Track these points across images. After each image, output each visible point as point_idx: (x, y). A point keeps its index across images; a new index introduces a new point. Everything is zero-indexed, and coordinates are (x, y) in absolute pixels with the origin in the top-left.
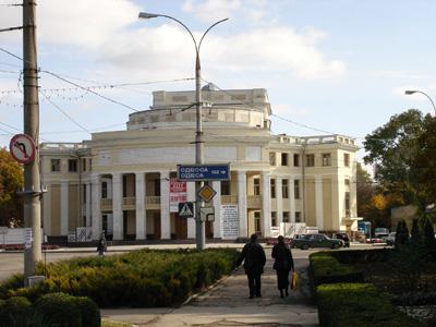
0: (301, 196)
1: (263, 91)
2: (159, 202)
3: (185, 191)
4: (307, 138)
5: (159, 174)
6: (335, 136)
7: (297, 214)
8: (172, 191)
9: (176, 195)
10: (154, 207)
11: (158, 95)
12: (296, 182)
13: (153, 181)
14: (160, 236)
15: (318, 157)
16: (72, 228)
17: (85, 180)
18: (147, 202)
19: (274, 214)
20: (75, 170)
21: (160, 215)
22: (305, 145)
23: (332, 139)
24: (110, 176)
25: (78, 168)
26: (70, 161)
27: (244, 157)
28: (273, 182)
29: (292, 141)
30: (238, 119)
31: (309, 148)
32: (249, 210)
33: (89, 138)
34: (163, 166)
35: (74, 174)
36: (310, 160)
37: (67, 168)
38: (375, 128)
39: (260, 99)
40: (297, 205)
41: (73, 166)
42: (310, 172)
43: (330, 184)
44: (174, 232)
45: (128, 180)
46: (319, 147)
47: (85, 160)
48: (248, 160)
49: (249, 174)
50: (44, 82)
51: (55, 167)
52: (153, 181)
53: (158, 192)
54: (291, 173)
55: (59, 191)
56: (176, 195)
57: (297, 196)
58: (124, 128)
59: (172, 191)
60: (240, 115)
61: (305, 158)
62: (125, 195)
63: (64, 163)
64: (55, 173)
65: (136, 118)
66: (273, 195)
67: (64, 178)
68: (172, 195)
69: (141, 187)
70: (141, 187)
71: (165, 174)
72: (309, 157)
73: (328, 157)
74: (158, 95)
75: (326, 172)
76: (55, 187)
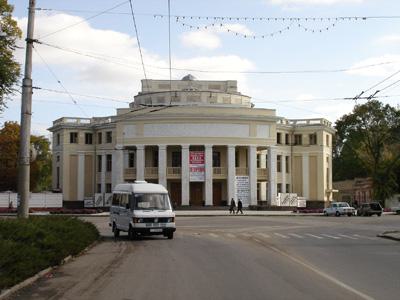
0: (290, 170)
1: (235, 82)
2: (180, 172)
3: (203, 162)
4: (295, 121)
6: (321, 119)
7: (287, 186)
8: (191, 163)
9: (195, 166)
10: (175, 177)
11: (145, 83)
12: (287, 158)
13: (175, 154)
16: (88, 193)
18: (169, 172)
19: (279, 186)
20: (91, 143)
21: (180, 183)
22: (294, 126)
23: (319, 122)
25: (93, 141)
26: (87, 135)
27: (255, 135)
28: (279, 157)
29: (284, 122)
30: (233, 101)
31: (299, 128)
33: (115, 114)
35: (89, 146)
36: (298, 140)
37: (84, 140)
38: (341, 115)
39: (233, 90)
40: (287, 178)
41: (89, 139)
42: (298, 150)
43: (315, 161)
46: (306, 128)
47: (100, 134)
48: (259, 136)
50: (36, 96)
51: (74, 138)
52: (175, 154)
53: (156, 163)
54: (284, 151)
55: (77, 160)
56: (195, 166)
57: (287, 171)
58: (128, 106)
59: (191, 163)
60: (220, 98)
63: (82, 136)
64: (73, 145)
65: (132, 105)
66: (279, 170)
67: (81, 147)
68: (191, 166)
69: (140, 156)
70: (140, 156)
71: (185, 146)
72: (297, 137)
73: (314, 139)
74: (145, 83)
75: (313, 149)
76: (74, 156)
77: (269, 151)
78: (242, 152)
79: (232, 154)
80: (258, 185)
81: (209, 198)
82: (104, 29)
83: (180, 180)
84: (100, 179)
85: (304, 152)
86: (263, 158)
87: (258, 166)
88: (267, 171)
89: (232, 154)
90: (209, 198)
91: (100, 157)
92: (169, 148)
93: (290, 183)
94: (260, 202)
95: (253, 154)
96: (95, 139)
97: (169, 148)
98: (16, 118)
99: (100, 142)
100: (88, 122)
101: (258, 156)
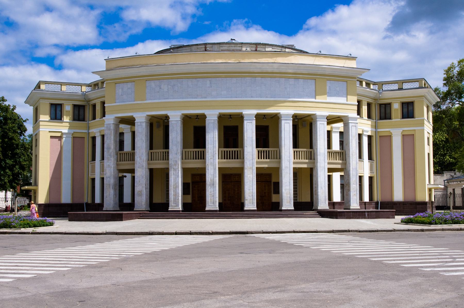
2: (202, 156)
5: (203, 117)
10: (194, 164)
12: (370, 137)
14: (205, 207)
15: (396, 107)
17: (95, 131)
18: (185, 157)
24: (131, 121)
28: (360, 136)
32: (330, 170)
34: (210, 106)
42: (386, 127)
43: (409, 141)
44: (221, 202)
45: (159, 126)
49: (331, 120)
57: (370, 158)
61: (378, 108)
62: (151, 147)
63: (68, 108)
66: (360, 157)
69: (213, 138)
70: (213, 138)
73: (408, 110)
75: (408, 126)
77: (346, 125)
78: (304, 127)
79: (287, 129)
80: (330, 177)
81: (176, 198)
82: (233, 126)
83: (204, 169)
84: (93, 171)
85: (396, 130)
86: (336, 139)
87: (329, 146)
88: (343, 154)
89: (287, 129)
90: (176, 198)
91: (94, 138)
92: (186, 119)
93: (374, 175)
94: (332, 204)
95: (321, 129)
96: (88, 113)
97: (186, 119)
98: (65, 121)
99: (94, 118)
100: (76, 90)
101: (329, 133)
